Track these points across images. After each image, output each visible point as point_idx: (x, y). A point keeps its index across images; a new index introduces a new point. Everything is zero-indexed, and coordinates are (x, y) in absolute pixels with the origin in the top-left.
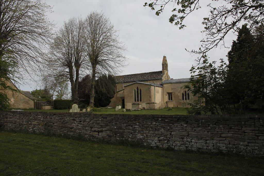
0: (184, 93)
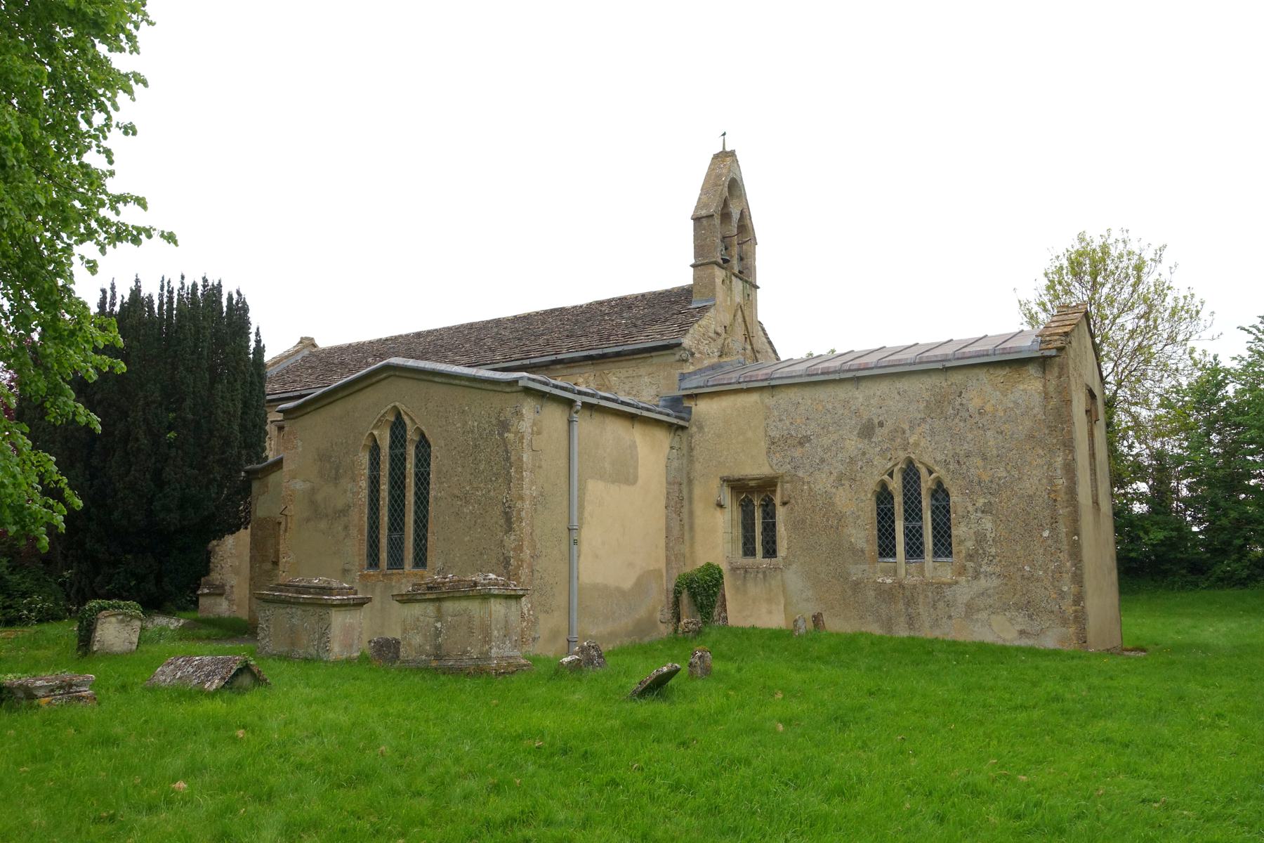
0: (896, 485)
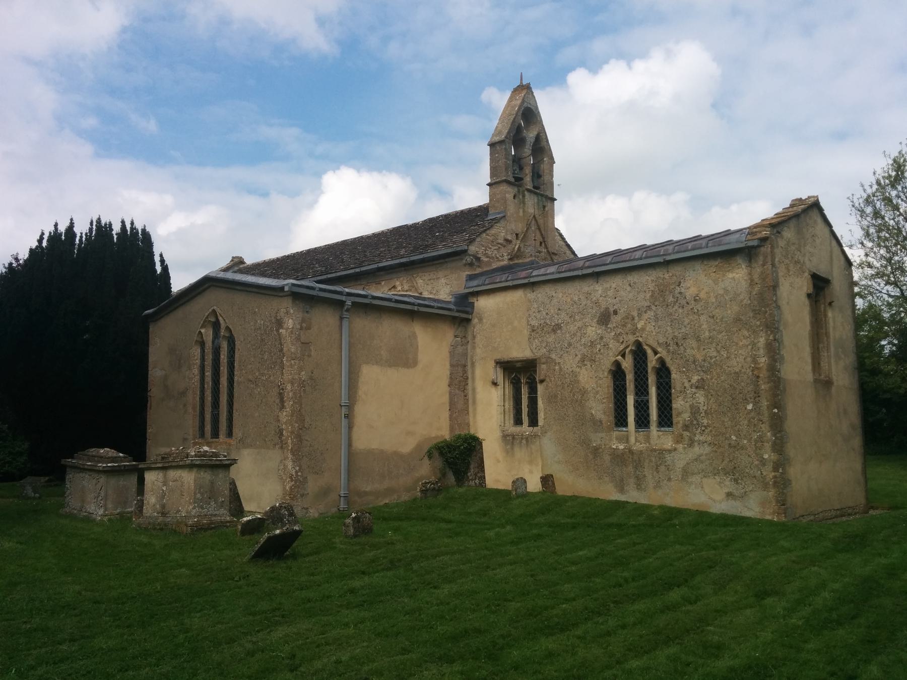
0: (627, 364)
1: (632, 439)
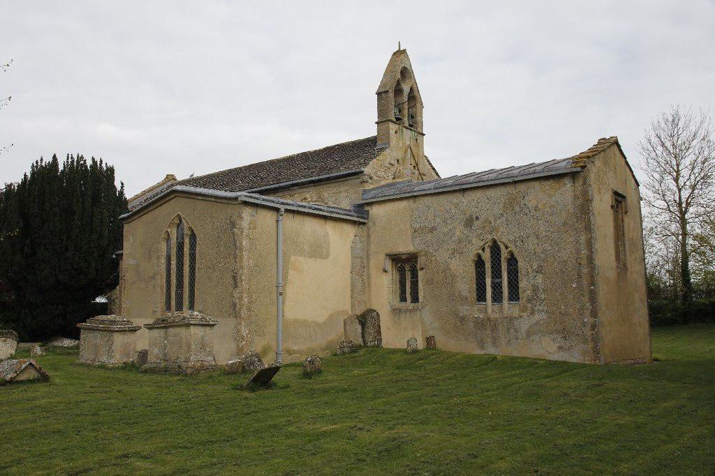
0: (486, 256)
1: (490, 311)
